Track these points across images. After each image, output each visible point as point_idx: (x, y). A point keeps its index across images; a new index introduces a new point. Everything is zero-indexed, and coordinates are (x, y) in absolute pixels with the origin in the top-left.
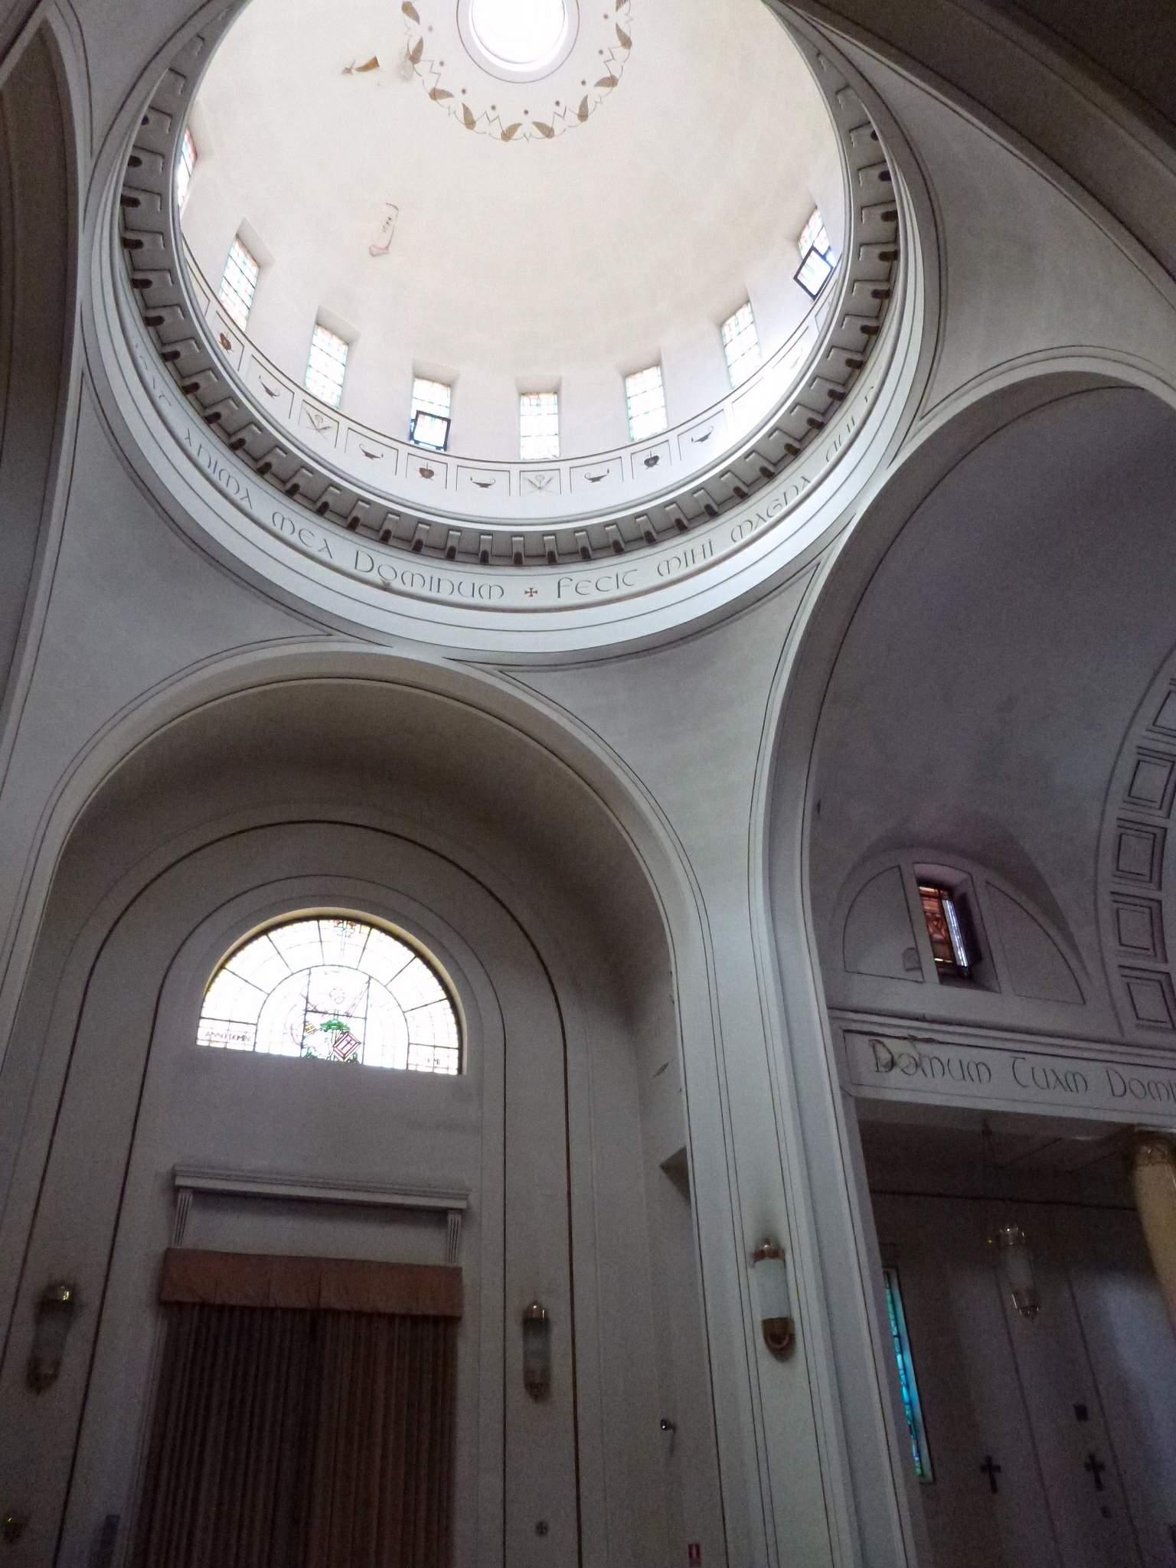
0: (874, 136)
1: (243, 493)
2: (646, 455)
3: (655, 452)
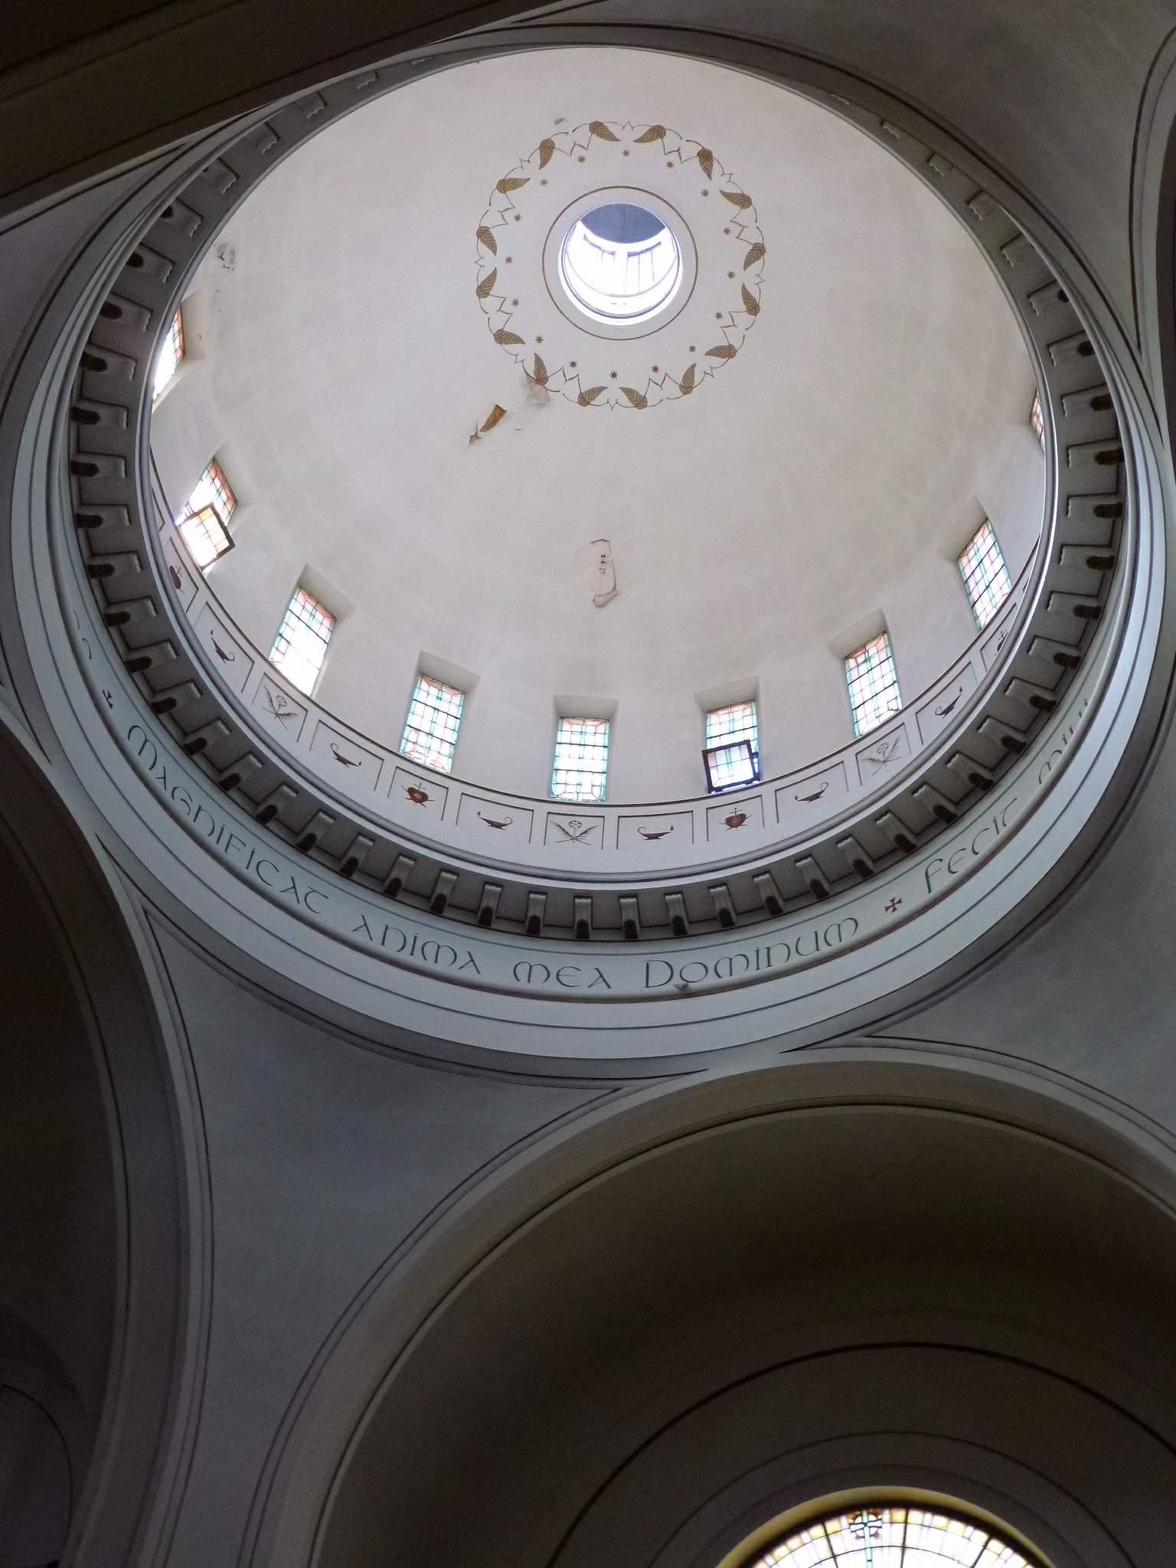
0: (1062, 296)
1: (158, 771)
2: (728, 812)
3: (742, 808)
